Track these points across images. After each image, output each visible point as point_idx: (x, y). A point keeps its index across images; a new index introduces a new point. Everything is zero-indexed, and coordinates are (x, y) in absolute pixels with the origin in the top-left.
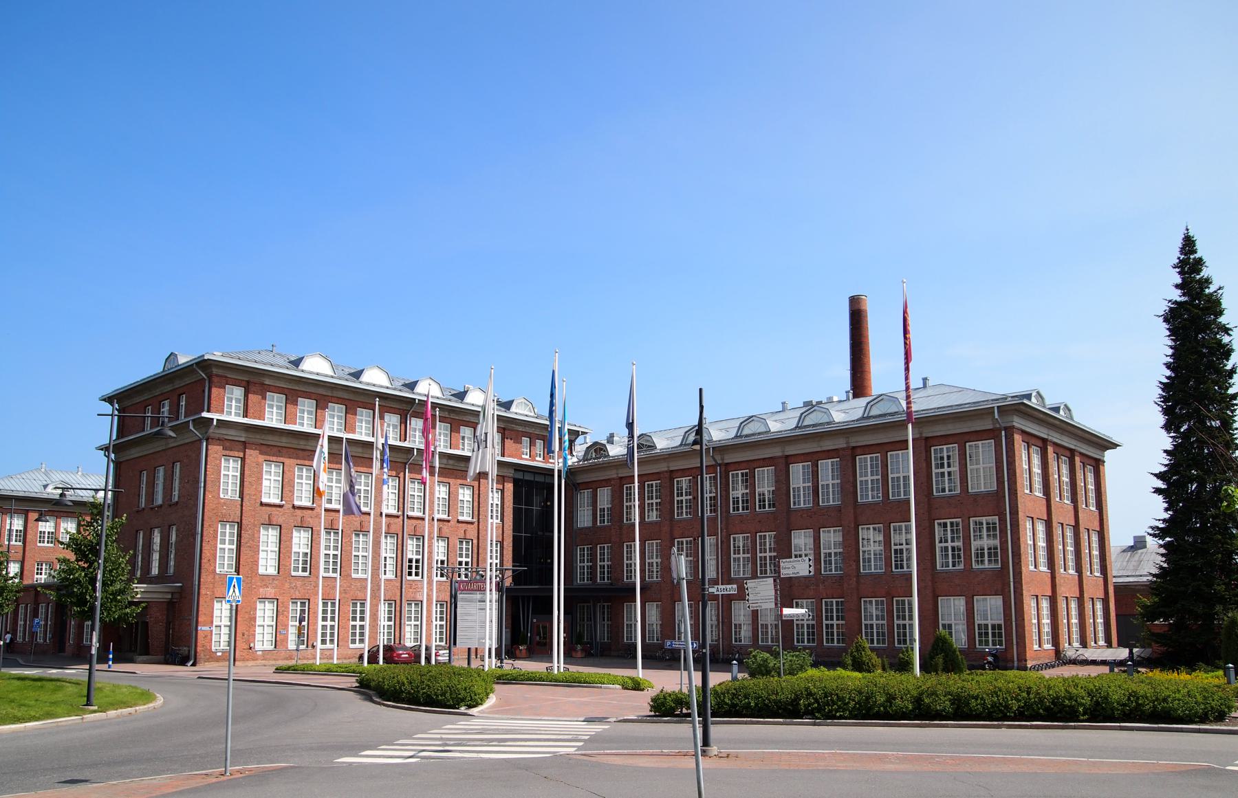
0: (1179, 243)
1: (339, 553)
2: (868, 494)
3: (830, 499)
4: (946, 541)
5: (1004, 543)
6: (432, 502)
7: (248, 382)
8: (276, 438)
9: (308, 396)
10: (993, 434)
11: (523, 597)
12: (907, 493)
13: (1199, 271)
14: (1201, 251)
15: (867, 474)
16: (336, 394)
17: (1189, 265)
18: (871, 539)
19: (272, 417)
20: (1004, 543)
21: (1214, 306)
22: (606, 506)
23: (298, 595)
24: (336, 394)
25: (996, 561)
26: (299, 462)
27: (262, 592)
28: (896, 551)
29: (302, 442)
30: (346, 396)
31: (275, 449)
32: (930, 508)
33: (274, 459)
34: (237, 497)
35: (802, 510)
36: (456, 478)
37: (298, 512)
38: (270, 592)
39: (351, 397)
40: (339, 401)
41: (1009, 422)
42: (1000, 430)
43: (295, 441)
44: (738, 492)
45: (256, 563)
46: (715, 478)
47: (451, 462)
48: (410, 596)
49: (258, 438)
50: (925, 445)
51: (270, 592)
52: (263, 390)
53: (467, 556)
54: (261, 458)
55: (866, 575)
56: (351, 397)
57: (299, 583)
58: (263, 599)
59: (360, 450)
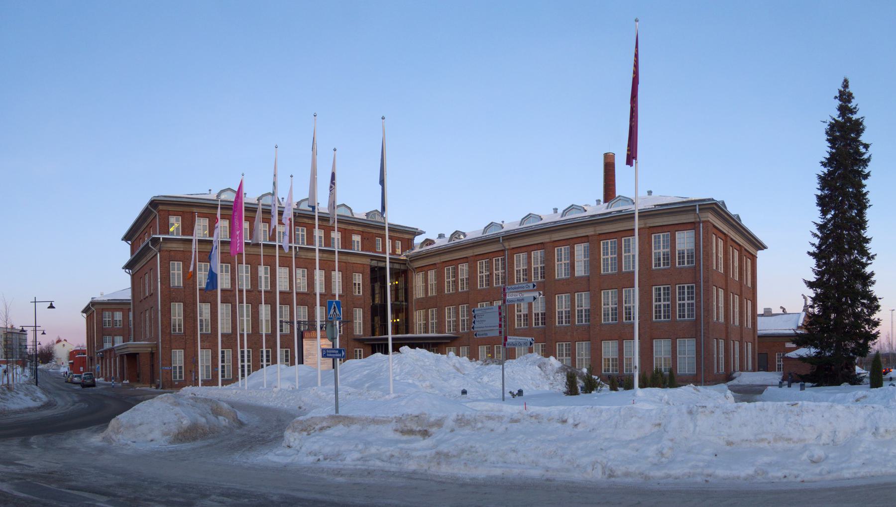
0: (842, 81)
2: (607, 267)
3: (432, 293)
4: (684, 300)
5: (698, 302)
10: (693, 226)
11: (378, 345)
12: (281, 308)
13: (850, 102)
14: (851, 89)
15: (607, 254)
17: (845, 97)
18: (608, 300)
20: (698, 302)
21: (858, 127)
22: (465, 276)
25: (692, 315)
28: (680, 305)
32: (649, 277)
35: (563, 279)
41: (706, 217)
42: (699, 223)
44: (448, 279)
45: (364, 312)
46: (504, 259)
47: (325, 255)
50: (647, 233)
55: (606, 324)
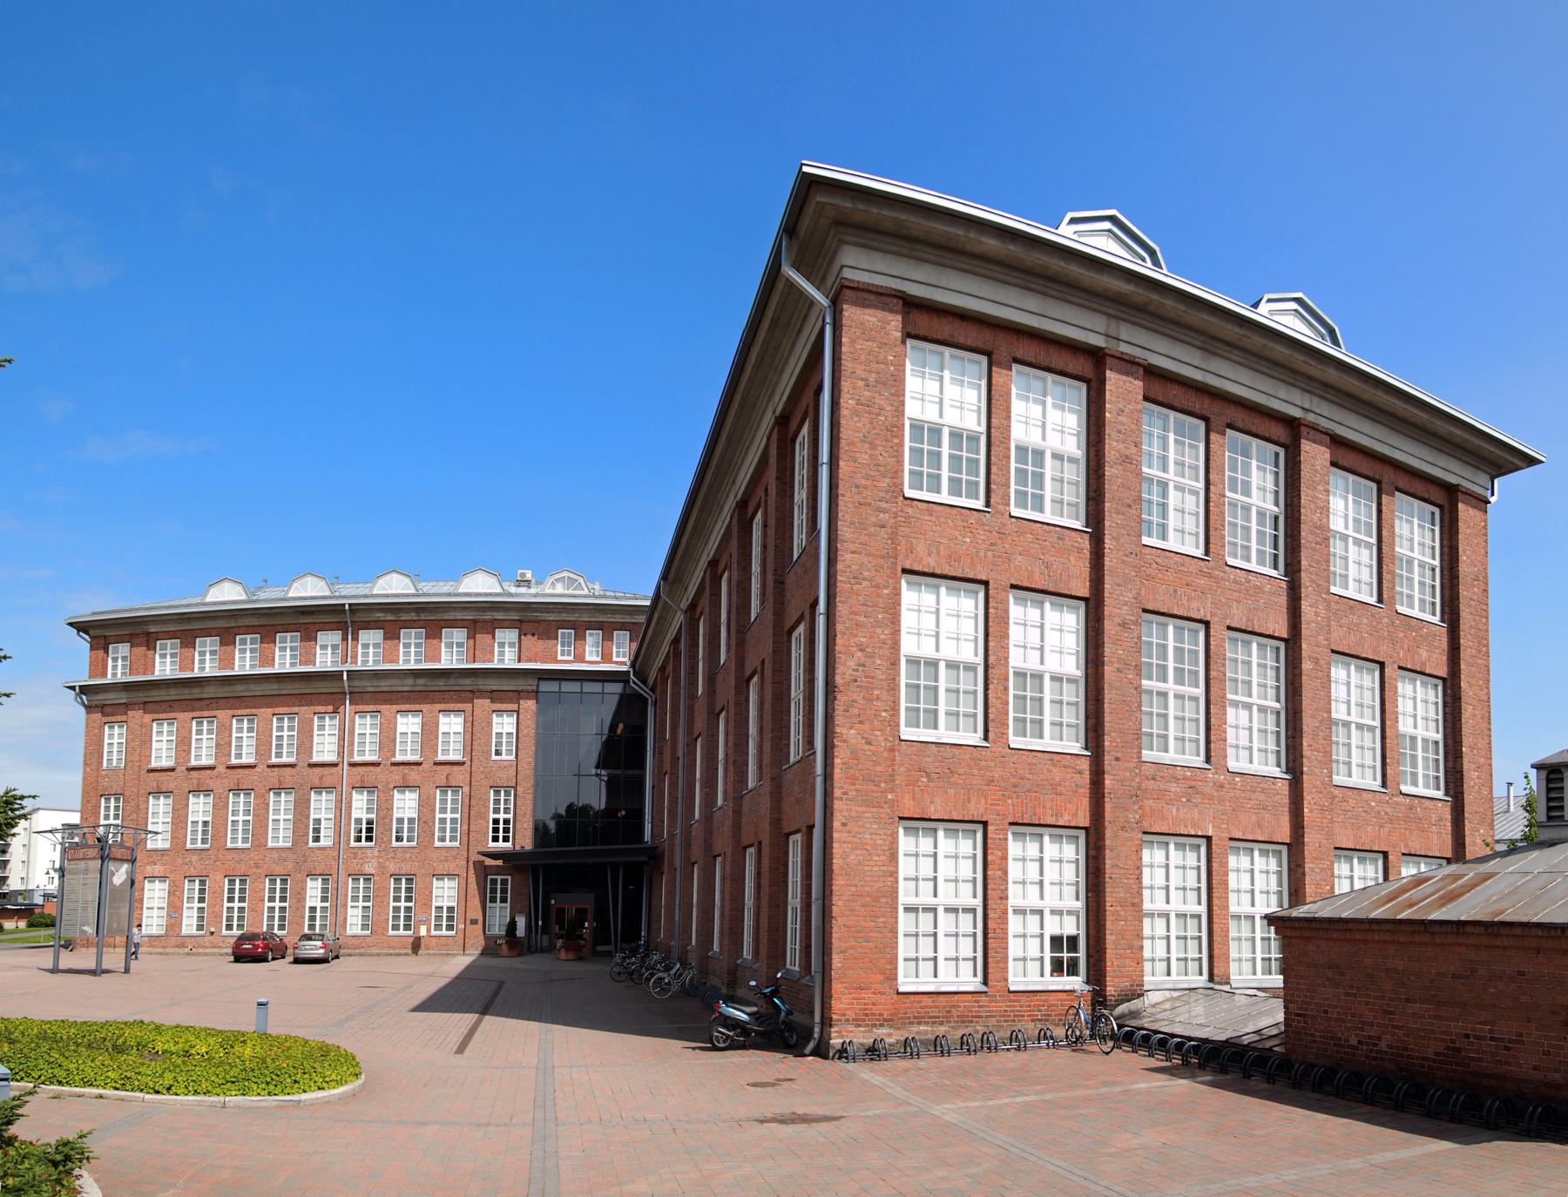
1: (510, 816)
6: (352, 744)
7: (475, 621)
8: (163, 692)
9: (207, 633)
16: (241, 622)
19: (164, 666)
23: (193, 872)
24: (241, 622)
26: (195, 714)
27: (149, 870)
29: (195, 691)
30: (255, 622)
31: (164, 706)
33: (164, 716)
34: (1074, 746)
36: (433, 702)
37: (317, 770)
38: (158, 869)
39: (263, 621)
40: (249, 630)
43: (187, 691)
47: (421, 681)
48: (354, 868)
49: (141, 696)
51: (158, 869)
52: (491, 627)
53: (454, 811)
54: (148, 718)
56: (263, 621)
57: (194, 858)
58: (152, 878)
59: (275, 686)
